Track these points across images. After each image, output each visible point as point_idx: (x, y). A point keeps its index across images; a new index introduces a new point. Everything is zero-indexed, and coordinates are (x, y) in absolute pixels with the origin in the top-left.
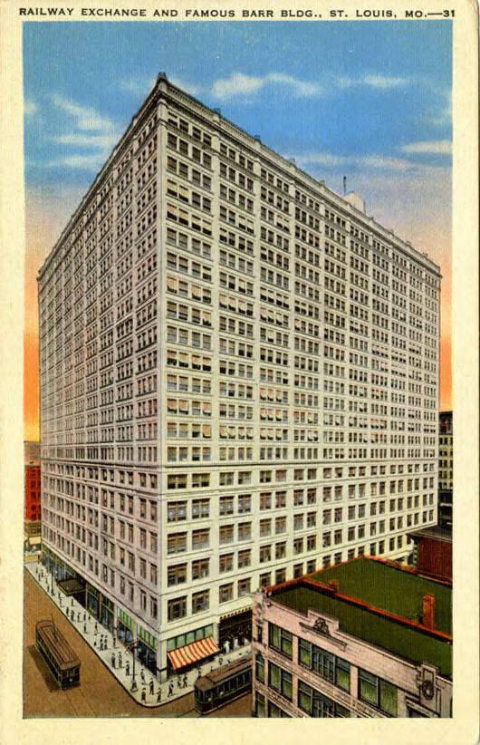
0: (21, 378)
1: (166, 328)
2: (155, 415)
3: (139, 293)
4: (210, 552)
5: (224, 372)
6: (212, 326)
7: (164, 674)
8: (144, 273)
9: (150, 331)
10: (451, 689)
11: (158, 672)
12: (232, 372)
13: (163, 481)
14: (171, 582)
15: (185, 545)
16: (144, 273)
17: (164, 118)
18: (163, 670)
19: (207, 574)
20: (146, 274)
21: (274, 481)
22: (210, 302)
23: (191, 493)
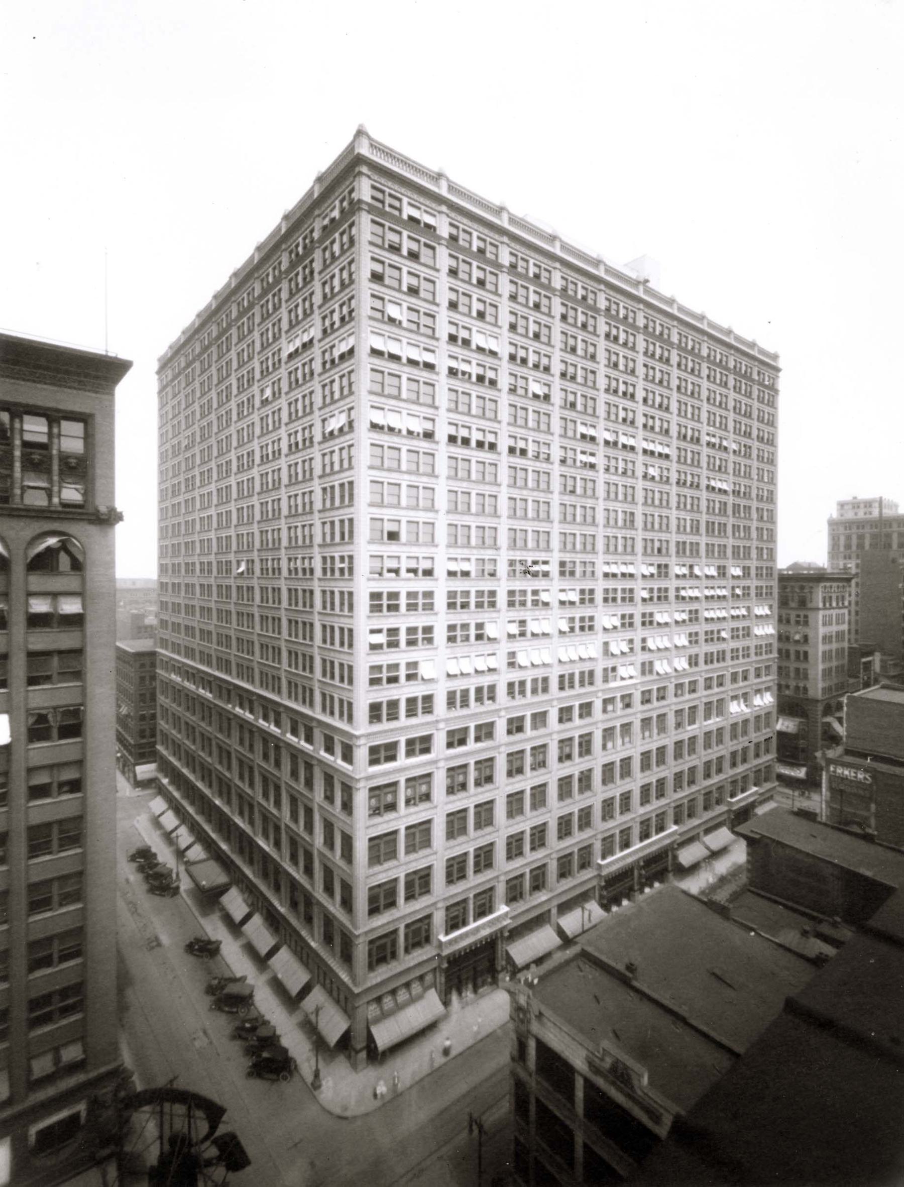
0: (102, 352)
1: (368, 483)
2: (351, 504)
3: (324, 353)
4: (433, 811)
5: (455, 608)
6: (437, 369)
7: (363, 1055)
8: (333, 324)
9: (341, 377)
10: (774, 379)
11: (353, 1054)
12: (465, 606)
13: (361, 800)
14: (376, 812)
15: (397, 713)
16: (333, 324)
17: (367, 198)
18: (361, 1050)
19: (428, 892)
20: (336, 326)
21: (529, 731)
22: (432, 609)
23: (406, 728)
